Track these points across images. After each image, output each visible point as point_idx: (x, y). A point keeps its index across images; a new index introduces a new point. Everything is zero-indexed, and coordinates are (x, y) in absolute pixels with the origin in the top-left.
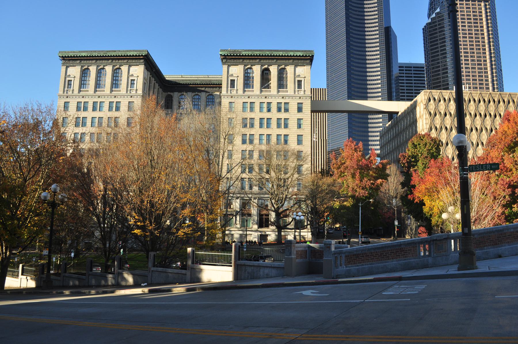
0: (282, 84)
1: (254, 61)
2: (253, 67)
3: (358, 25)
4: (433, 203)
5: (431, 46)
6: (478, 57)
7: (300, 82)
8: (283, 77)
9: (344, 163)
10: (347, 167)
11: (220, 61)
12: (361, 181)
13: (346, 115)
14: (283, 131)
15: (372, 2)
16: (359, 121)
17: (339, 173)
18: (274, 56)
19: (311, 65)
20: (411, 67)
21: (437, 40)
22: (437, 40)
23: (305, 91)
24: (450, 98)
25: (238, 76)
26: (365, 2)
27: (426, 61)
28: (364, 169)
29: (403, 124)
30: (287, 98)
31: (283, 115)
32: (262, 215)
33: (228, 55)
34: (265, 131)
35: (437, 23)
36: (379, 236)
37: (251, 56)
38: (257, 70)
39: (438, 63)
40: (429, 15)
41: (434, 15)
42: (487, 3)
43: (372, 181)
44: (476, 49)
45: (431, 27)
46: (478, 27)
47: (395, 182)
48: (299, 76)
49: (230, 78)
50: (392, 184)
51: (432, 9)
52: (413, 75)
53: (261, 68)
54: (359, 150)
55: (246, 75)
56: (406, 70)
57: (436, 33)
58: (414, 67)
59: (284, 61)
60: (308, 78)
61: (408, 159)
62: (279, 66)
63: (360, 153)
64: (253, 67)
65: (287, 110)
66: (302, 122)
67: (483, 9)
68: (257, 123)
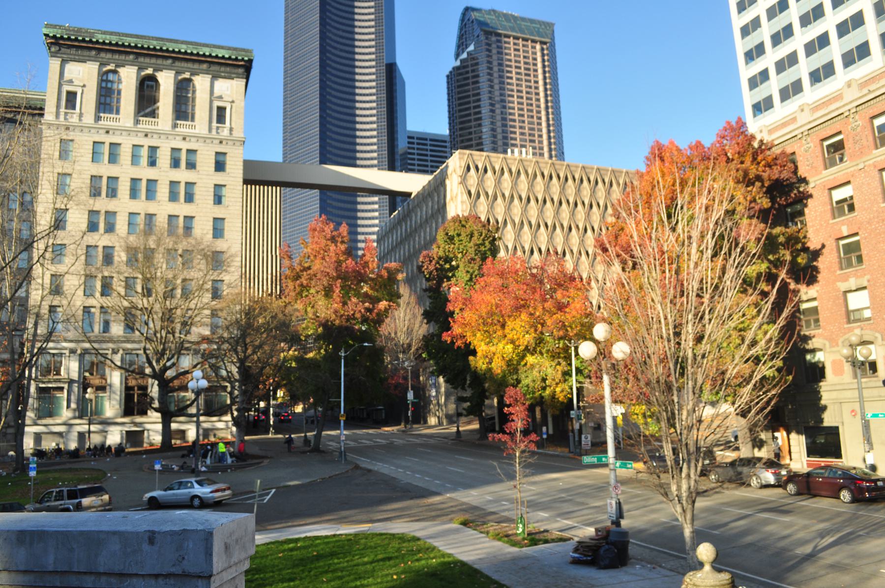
0: (183, 109)
1: (123, 57)
2: (121, 70)
3: (342, 102)
4: (493, 349)
5: (460, 105)
6: (530, 129)
7: (221, 110)
8: (187, 98)
9: (309, 268)
10: (315, 275)
11: (45, 48)
12: (344, 304)
13: (316, 192)
14: (182, 209)
15: (366, 4)
16: (340, 202)
17: (298, 289)
18: (167, 51)
19: (247, 78)
20: (426, 139)
21: (469, 96)
22: (469, 96)
23: (81, 115)
24: (502, 169)
25: (84, 86)
26: (356, 4)
27: (450, 130)
28: (349, 279)
29: (418, 217)
30: (193, 139)
31: (183, 175)
32: (132, 388)
33: (62, 38)
34: (141, 206)
35: (470, 69)
36: (378, 423)
37: (117, 44)
38: (128, 78)
39: (470, 133)
40: (457, 55)
41: (464, 56)
42: (545, 47)
43: (367, 304)
44: (528, 116)
45: (461, 74)
46: (530, 81)
47: (407, 318)
48: (71, 82)
49: (66, 88)
50: (405, 322)
51: (461, 45)
52: (429, 158)
53: (138, 73)
54: (340, 239)
55: (104, 85)
56: (418, 144)
57: (468, 84)
58: (431, 140)
59: (190, 65)
60: (240, 103)
61: (438, 263)
62: (178, 73)
63: (343, 247)
64: (121, 70)
65: (191, 166)
66: (224, 191)
67: (539, 54)
68: (124, 188)
